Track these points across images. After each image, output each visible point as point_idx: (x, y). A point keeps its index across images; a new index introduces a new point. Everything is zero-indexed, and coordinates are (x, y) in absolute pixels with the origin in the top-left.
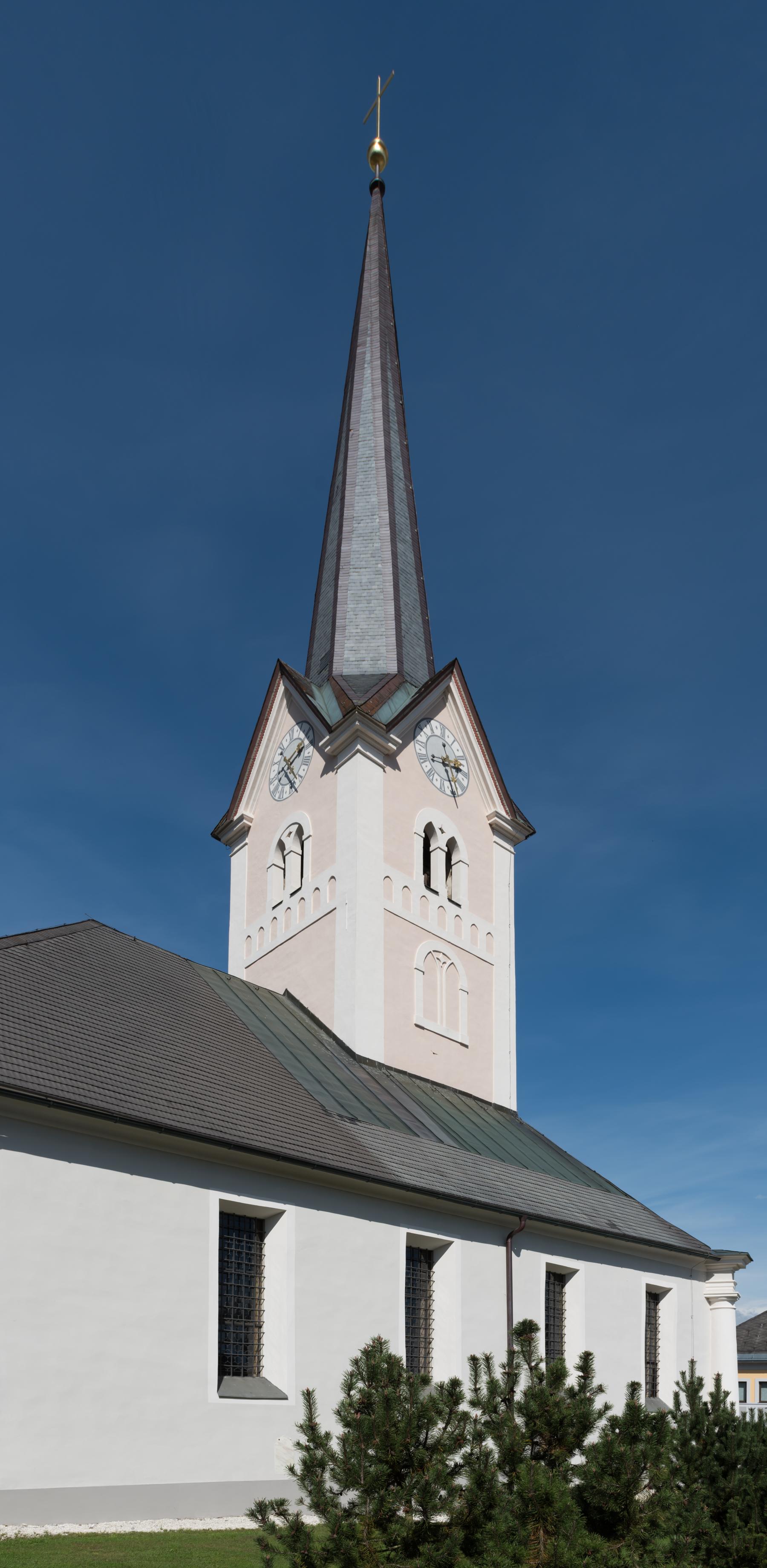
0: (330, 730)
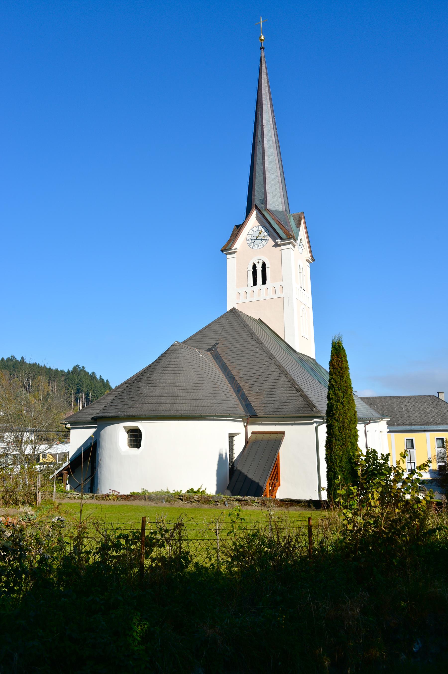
0: (281, 238)
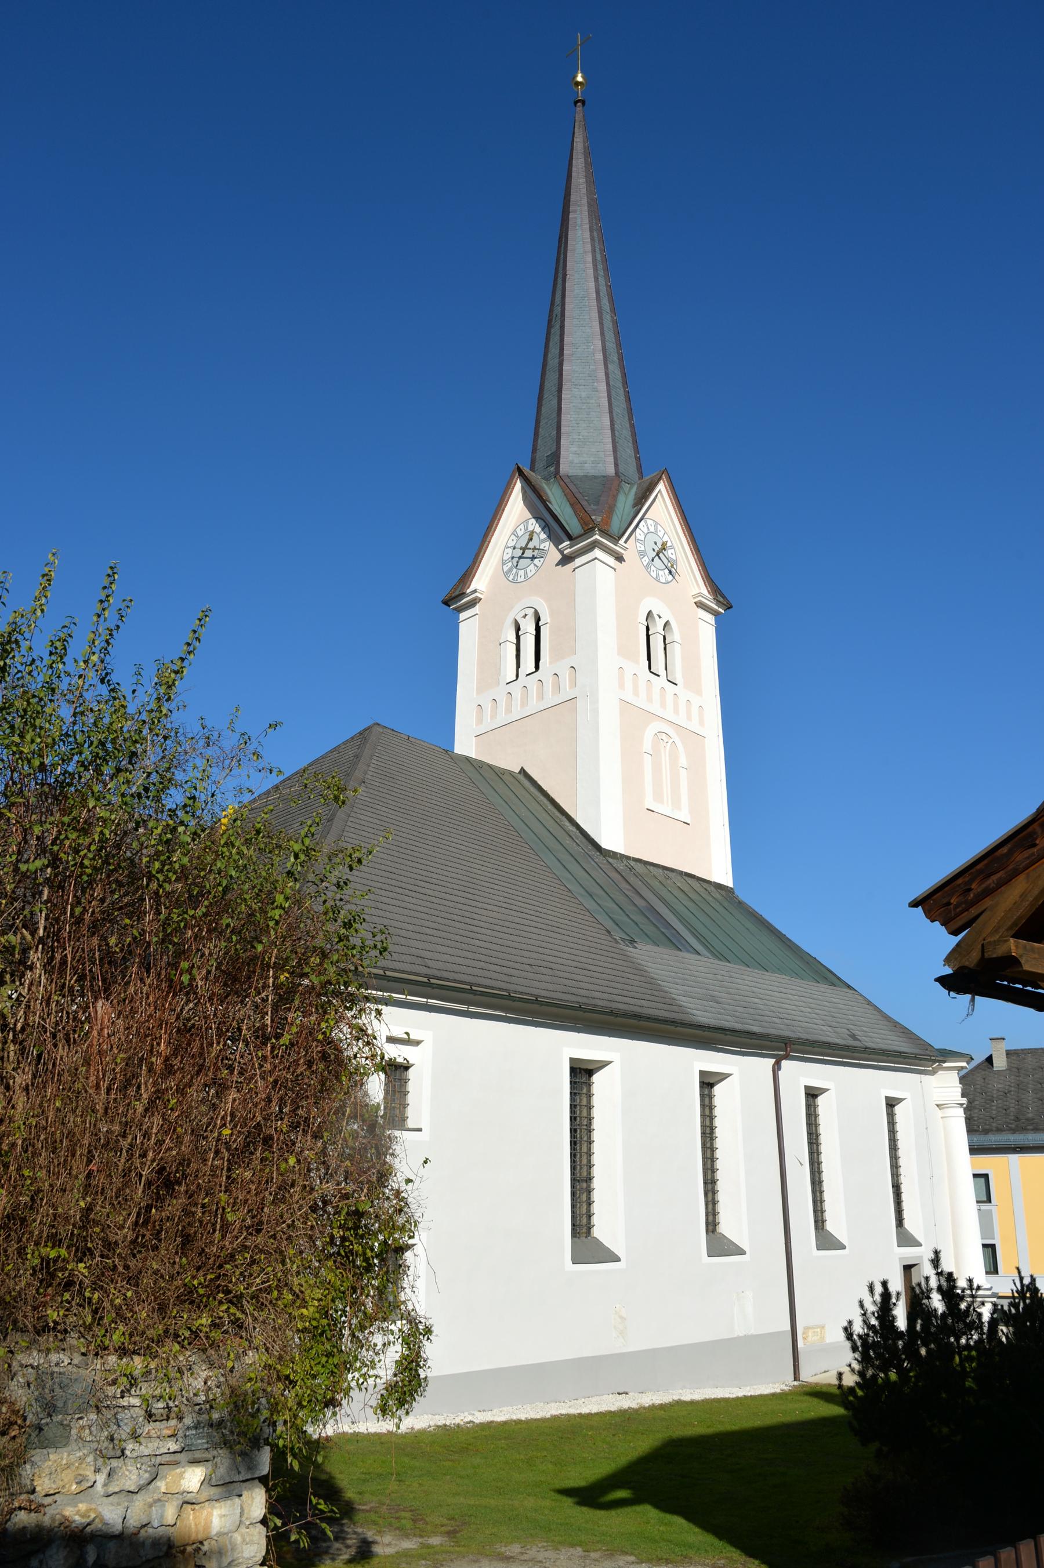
0: (570, 538)
